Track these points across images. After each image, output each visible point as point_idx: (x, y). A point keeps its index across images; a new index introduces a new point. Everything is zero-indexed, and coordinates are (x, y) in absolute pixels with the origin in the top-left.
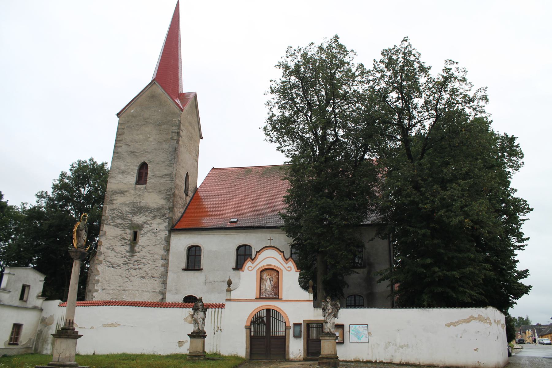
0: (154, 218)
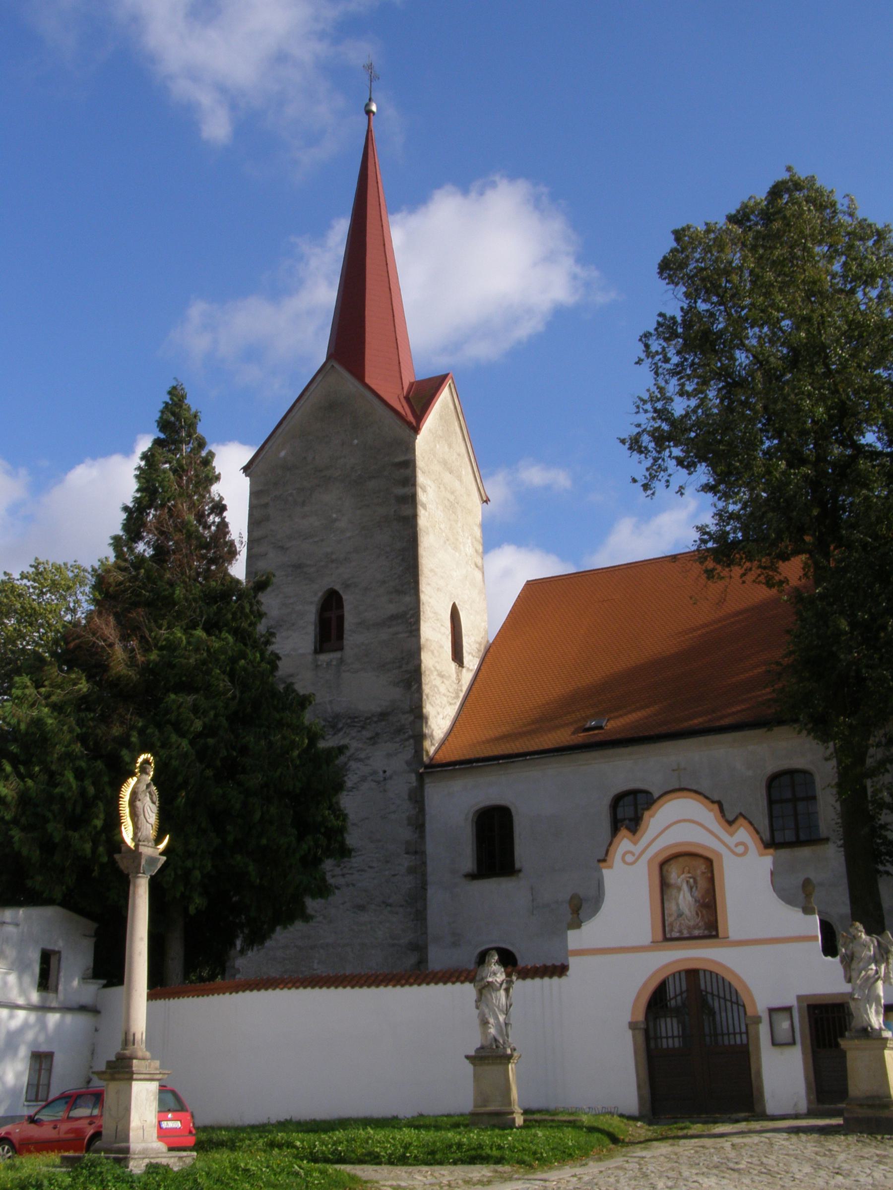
0: (374, 740)
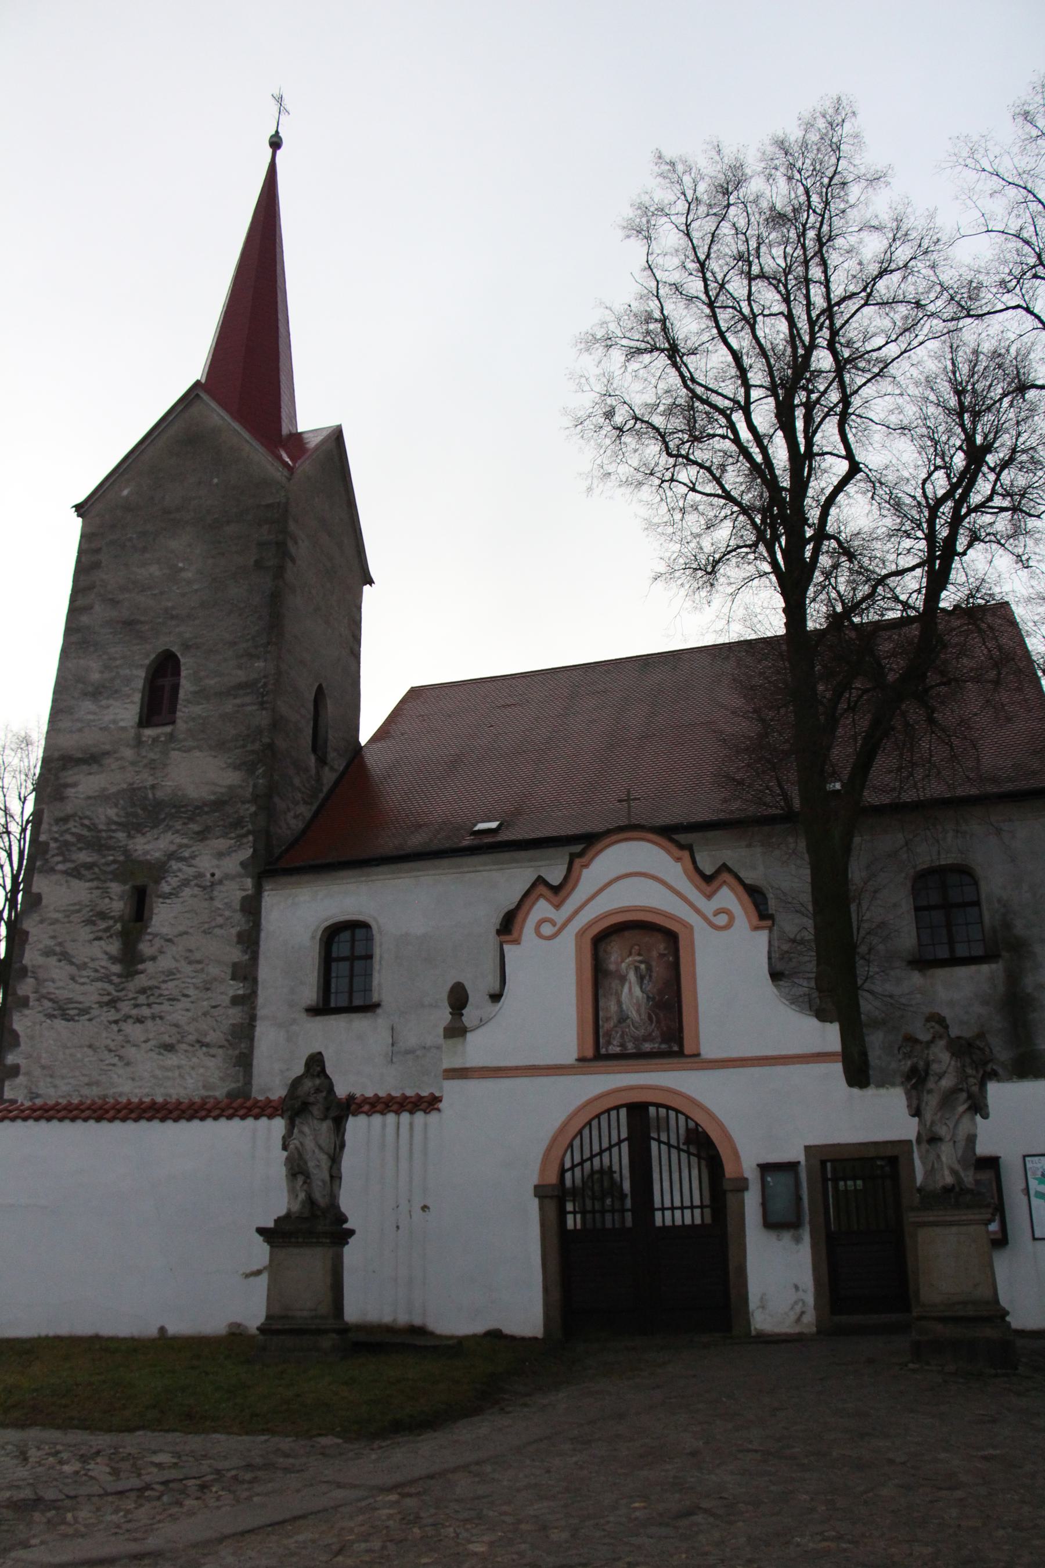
0: (202, 835)
